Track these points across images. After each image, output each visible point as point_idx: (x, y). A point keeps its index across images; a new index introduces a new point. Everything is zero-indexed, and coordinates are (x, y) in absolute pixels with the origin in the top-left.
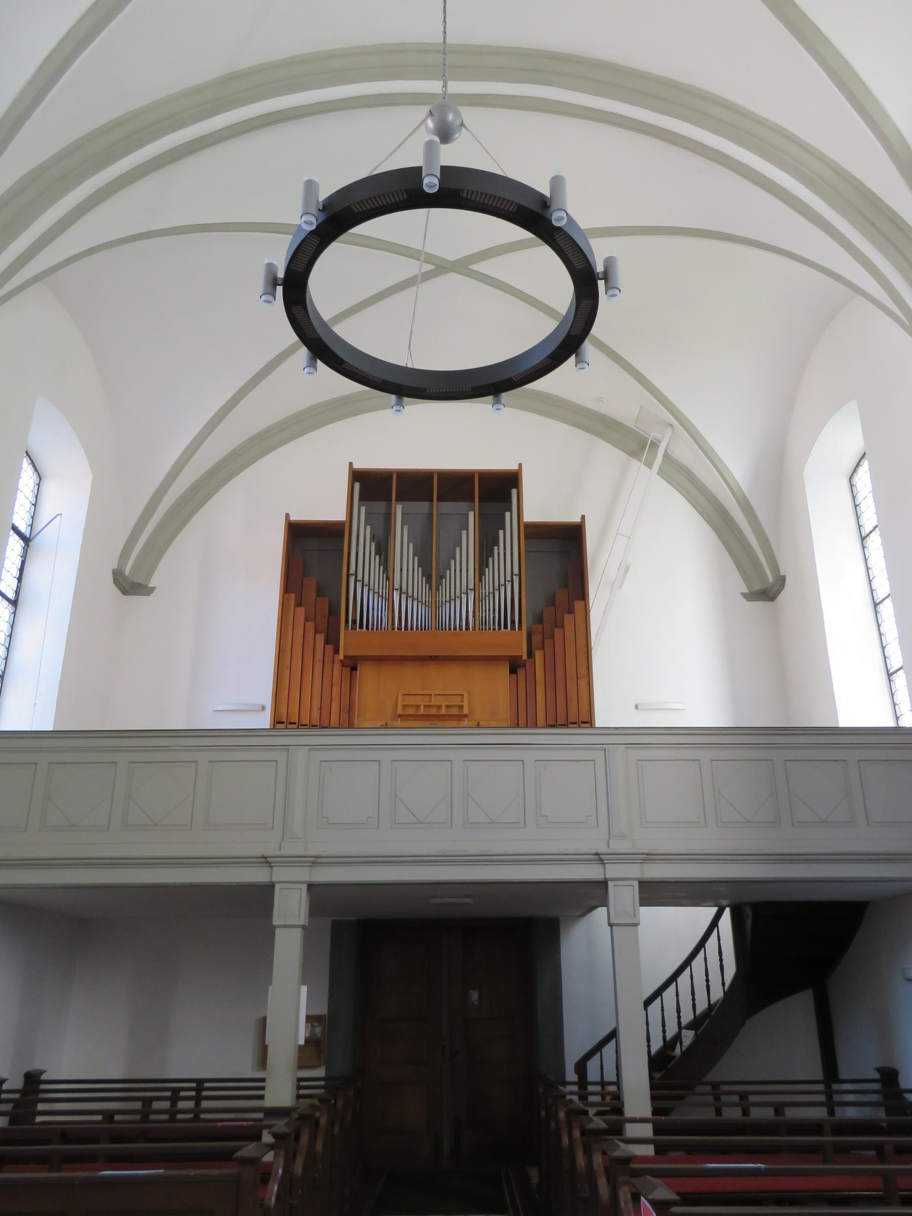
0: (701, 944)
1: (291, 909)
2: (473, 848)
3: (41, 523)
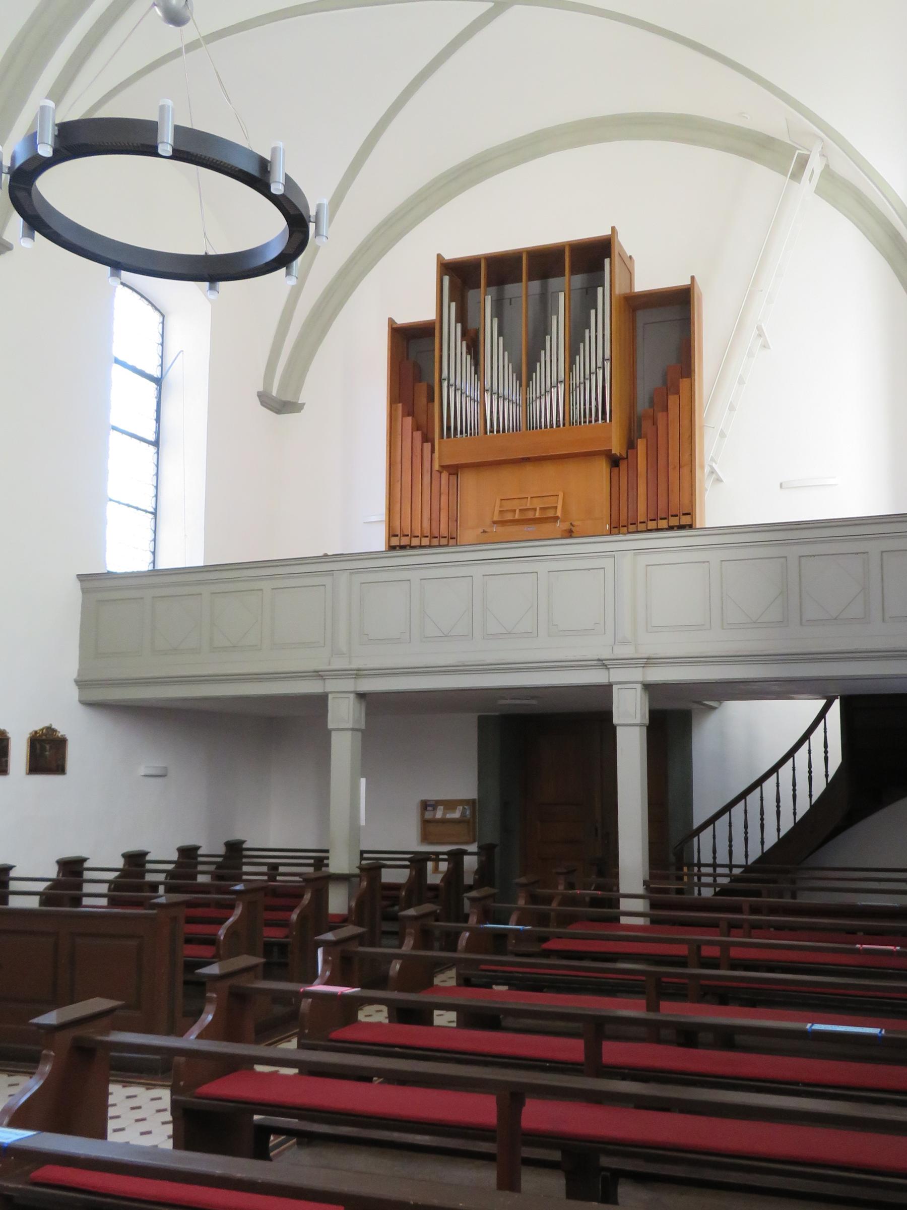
1: (343, 714)
2: (490, 658)
3: (167, 363)
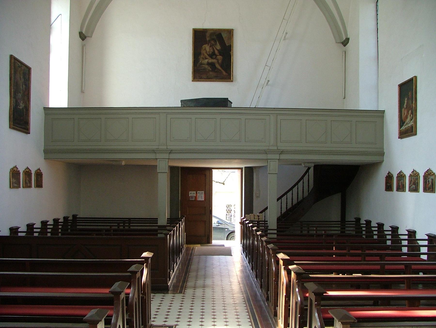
0: (302, 178)
1: (163, 167)
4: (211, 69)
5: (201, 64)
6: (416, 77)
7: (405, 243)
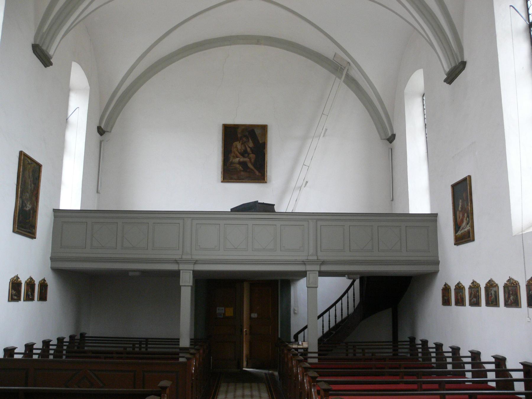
1: (187, 280)
4: (242, 169)
5: (232, 163)
6: (470, 177)
7: (449, 360)
